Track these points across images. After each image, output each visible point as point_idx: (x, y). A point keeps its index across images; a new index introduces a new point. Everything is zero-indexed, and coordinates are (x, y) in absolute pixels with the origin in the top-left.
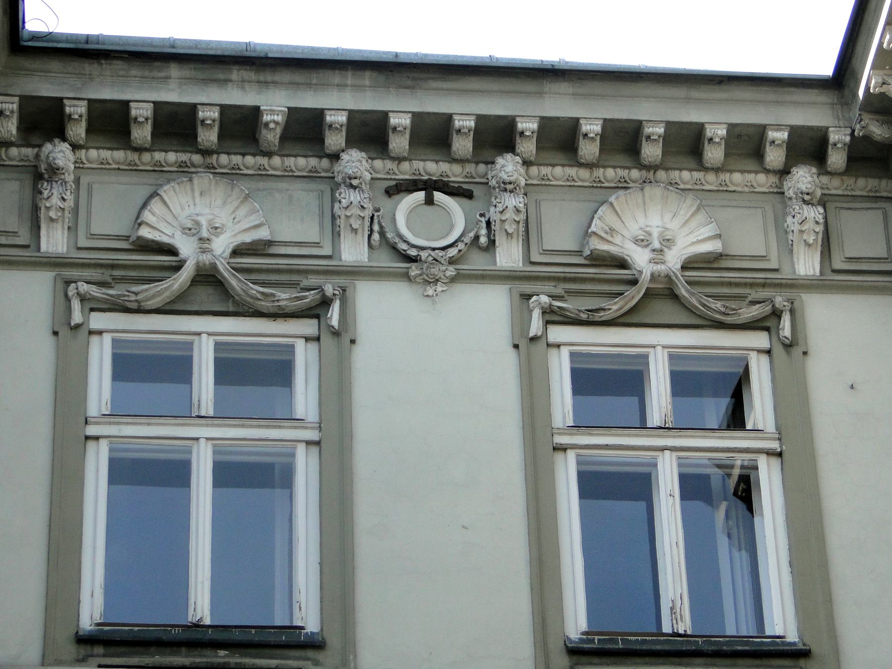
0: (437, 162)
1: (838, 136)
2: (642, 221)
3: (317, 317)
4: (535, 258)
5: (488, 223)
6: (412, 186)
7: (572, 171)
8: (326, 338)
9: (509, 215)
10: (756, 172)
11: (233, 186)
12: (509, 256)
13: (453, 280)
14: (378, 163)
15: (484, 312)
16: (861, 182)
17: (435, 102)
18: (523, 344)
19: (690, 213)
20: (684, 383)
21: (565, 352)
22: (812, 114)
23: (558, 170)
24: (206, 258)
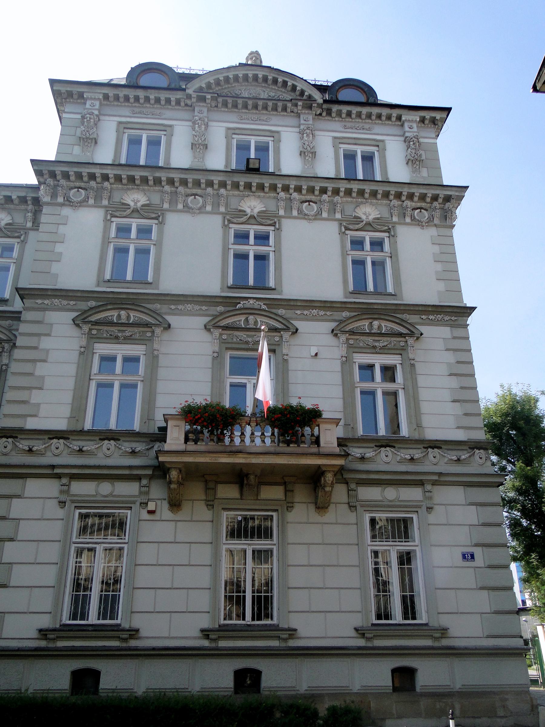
2: (133, 197)
3: (157, 219)
6: (306, 202)
8: (391, 237)
13: (199, 213)
14: (186, 190)
15: (218, 220)
17: (93, 170)
20: (372, 244)
21: (233, 229)
24: (252, 214)
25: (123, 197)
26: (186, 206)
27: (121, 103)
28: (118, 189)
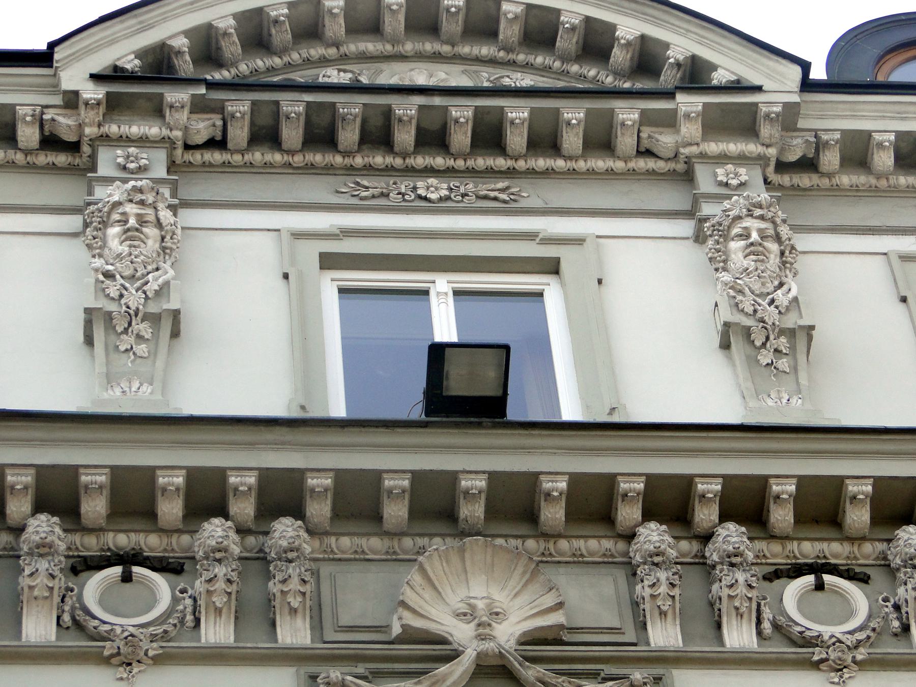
4: (330, 635)
5: (897, 607)
6: (797, 571)
12: (294, 633)
19: (521, 584)
25: (410, 597)
26: (76, 623)
27: (346, 154)
28: (361, 559)
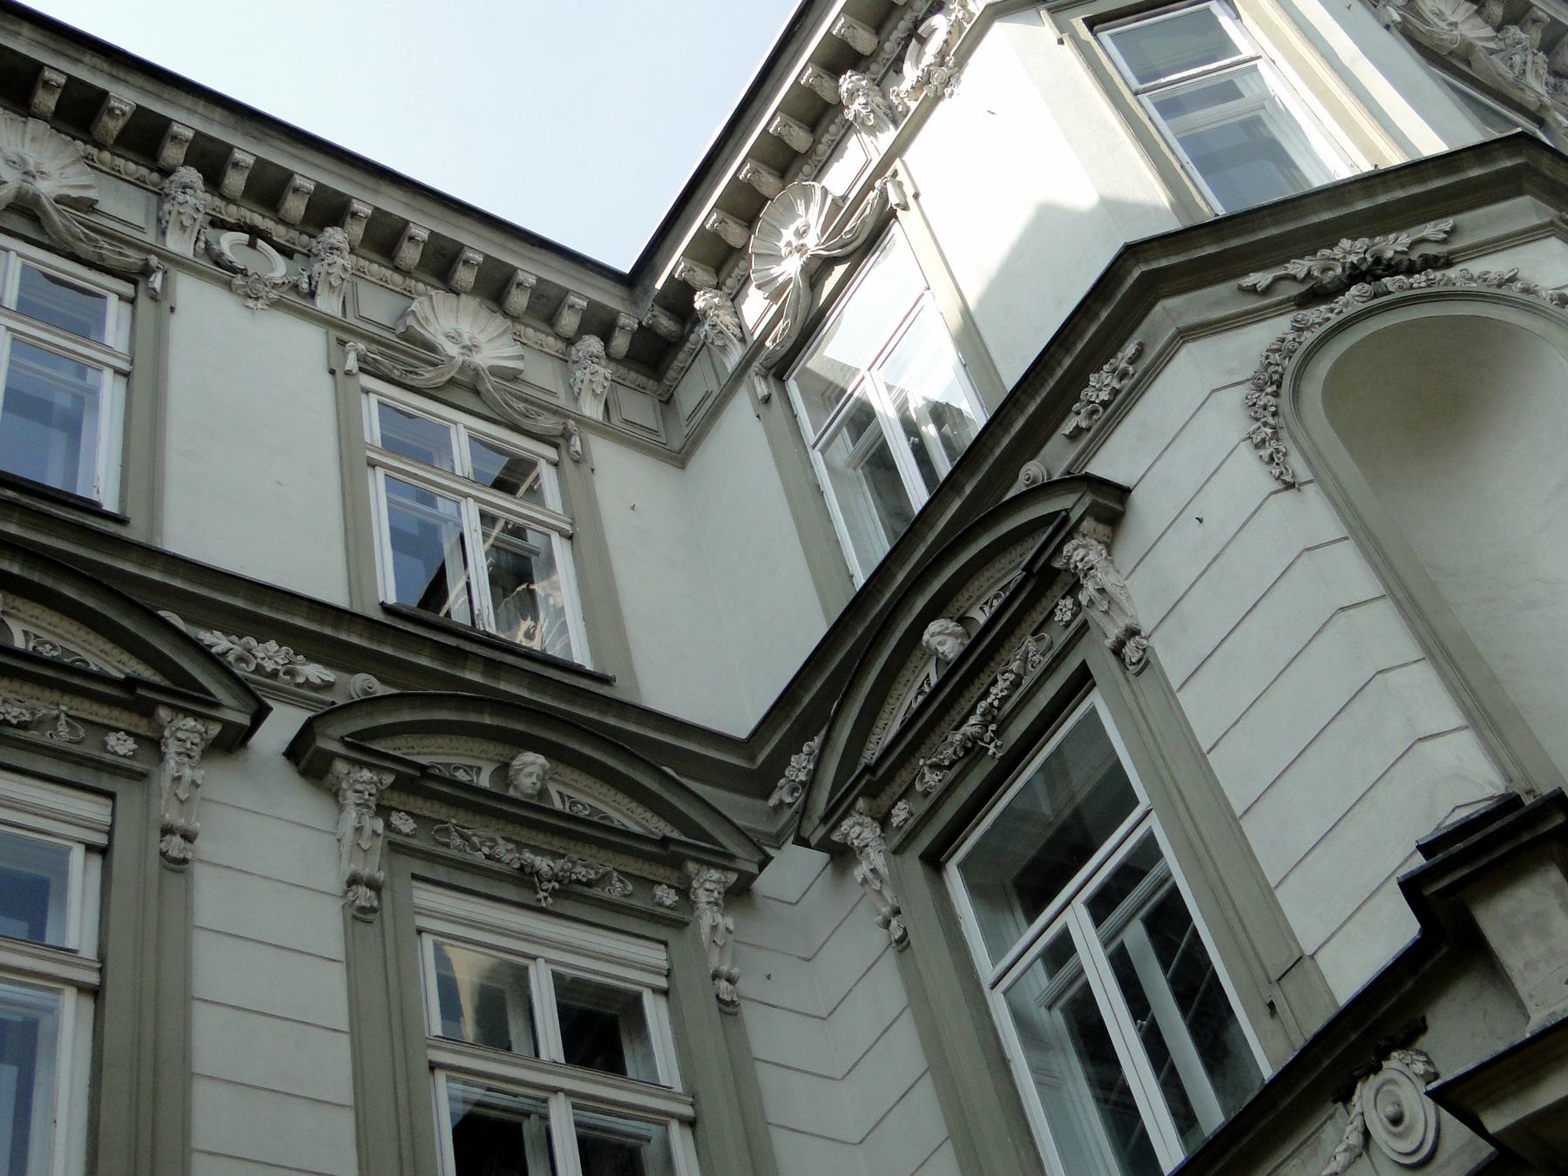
0: (264, 217)
1: (628, 321)
5: (310, 278)
7: (388, 273)
8: (143, 302)
9: (336, 270)
10: (548, 335)
11: (67, 144)
16: (633, 375)
18: (339, 373)
22: (610, 298)
23: (375, 267)
